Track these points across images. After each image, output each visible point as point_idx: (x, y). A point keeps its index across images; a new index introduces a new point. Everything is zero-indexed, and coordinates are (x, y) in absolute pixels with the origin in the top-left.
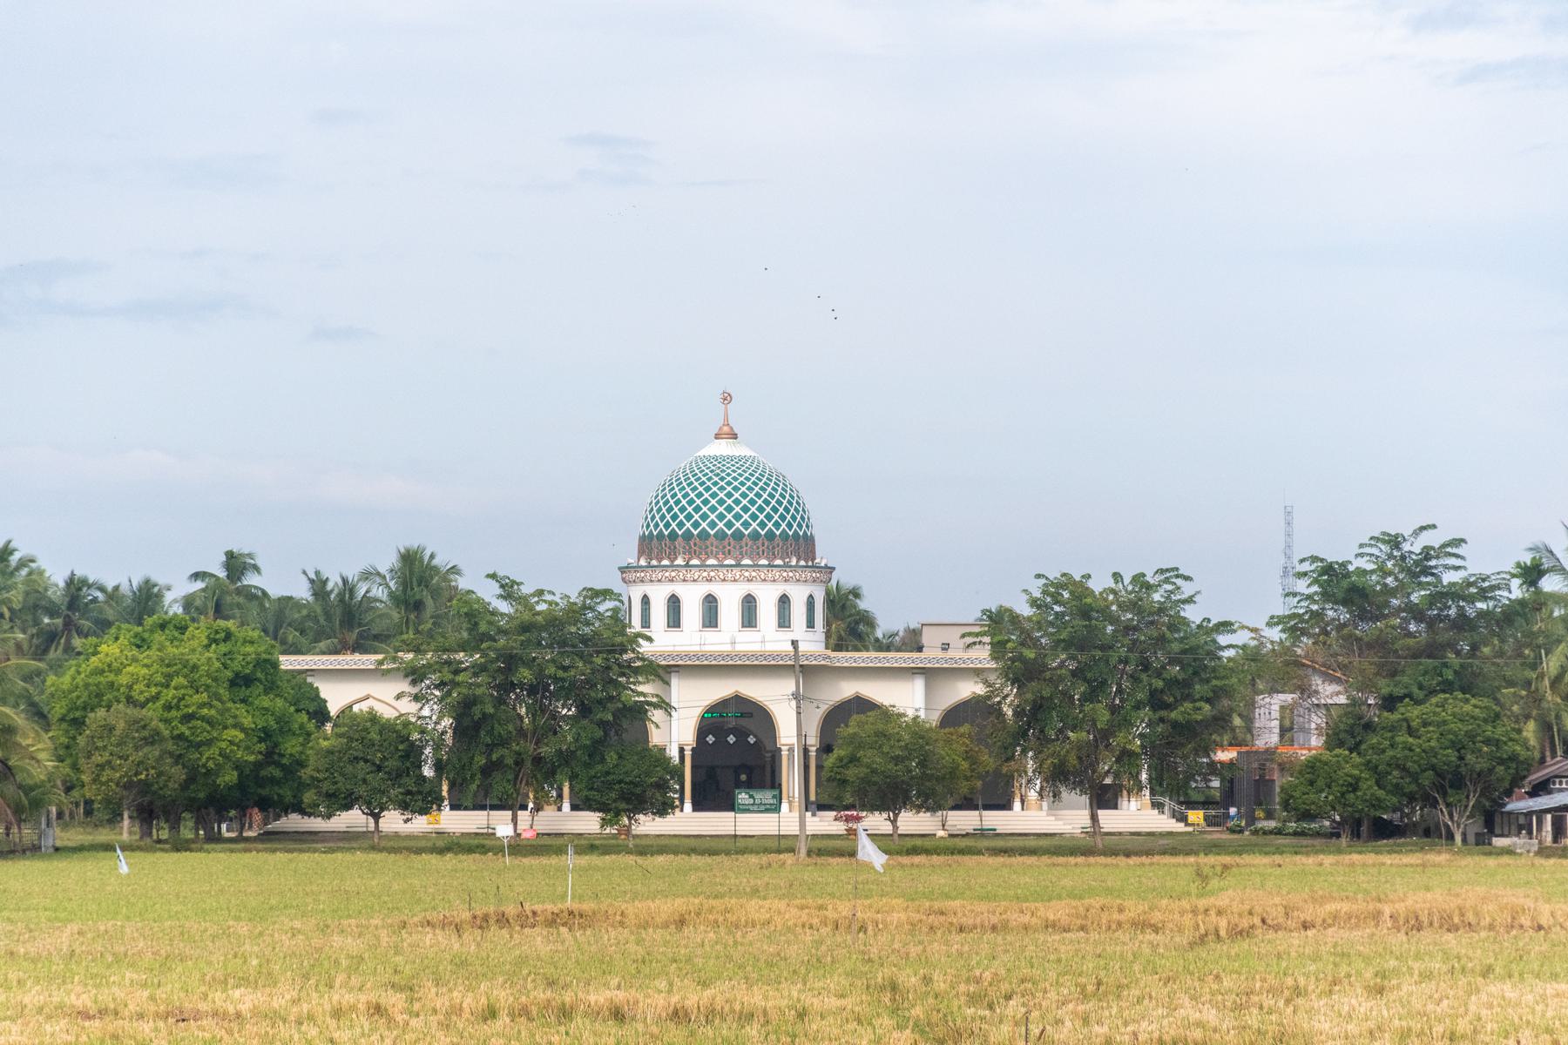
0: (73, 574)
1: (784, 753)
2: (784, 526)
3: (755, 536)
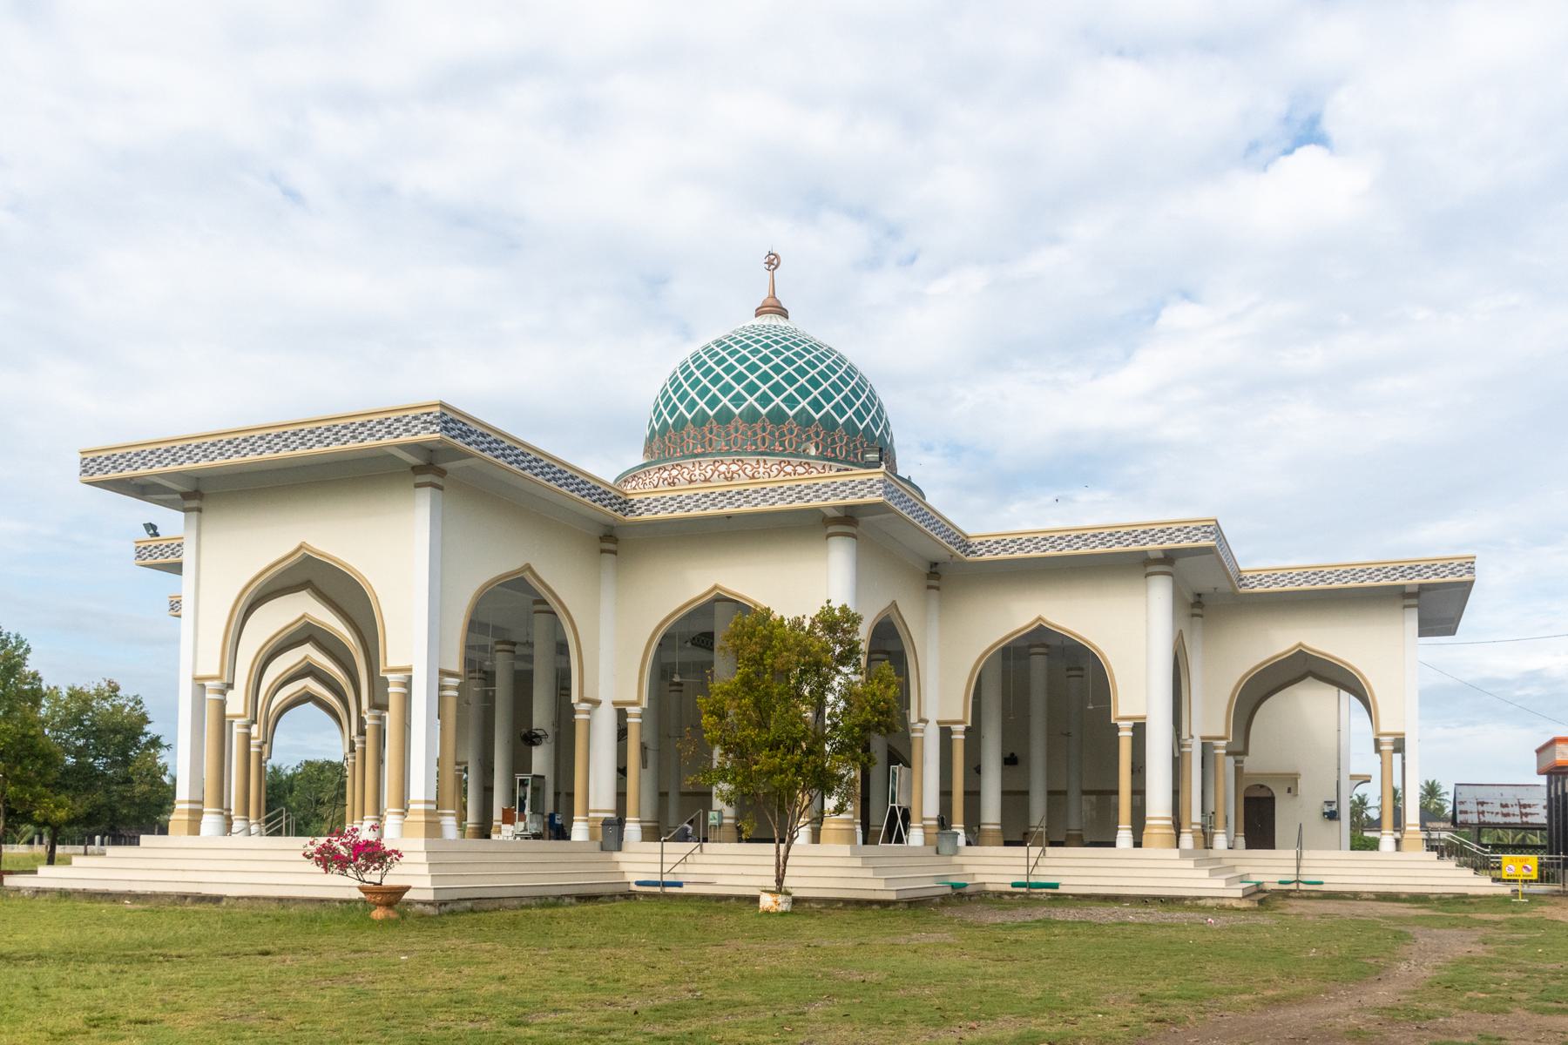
3: (804, 420)
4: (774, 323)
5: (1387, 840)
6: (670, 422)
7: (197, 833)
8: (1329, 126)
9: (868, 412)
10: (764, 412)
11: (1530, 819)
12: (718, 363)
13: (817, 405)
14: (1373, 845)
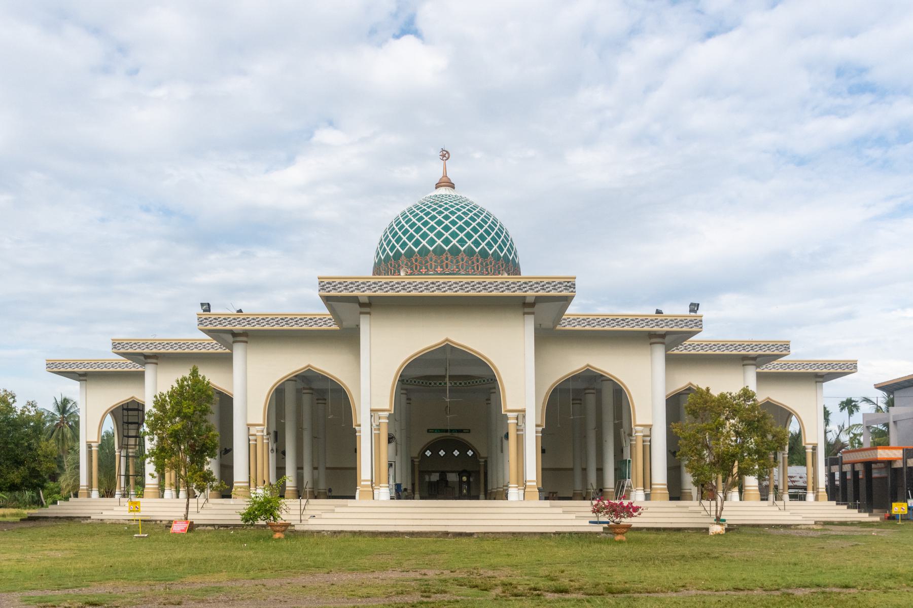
0: (651, 354)
1: (809, 451)
2: (495, 247)
3: (470, 252)
4: (448, 193)
5: (810, 496)
6: (391, 255)
7: (163, 497)
8: (421, 24)
9: (505, 246)
10: (447, 248)
11: (796, 484)
12: (419, 220)
13: (447, 242)
14: (803, 498)
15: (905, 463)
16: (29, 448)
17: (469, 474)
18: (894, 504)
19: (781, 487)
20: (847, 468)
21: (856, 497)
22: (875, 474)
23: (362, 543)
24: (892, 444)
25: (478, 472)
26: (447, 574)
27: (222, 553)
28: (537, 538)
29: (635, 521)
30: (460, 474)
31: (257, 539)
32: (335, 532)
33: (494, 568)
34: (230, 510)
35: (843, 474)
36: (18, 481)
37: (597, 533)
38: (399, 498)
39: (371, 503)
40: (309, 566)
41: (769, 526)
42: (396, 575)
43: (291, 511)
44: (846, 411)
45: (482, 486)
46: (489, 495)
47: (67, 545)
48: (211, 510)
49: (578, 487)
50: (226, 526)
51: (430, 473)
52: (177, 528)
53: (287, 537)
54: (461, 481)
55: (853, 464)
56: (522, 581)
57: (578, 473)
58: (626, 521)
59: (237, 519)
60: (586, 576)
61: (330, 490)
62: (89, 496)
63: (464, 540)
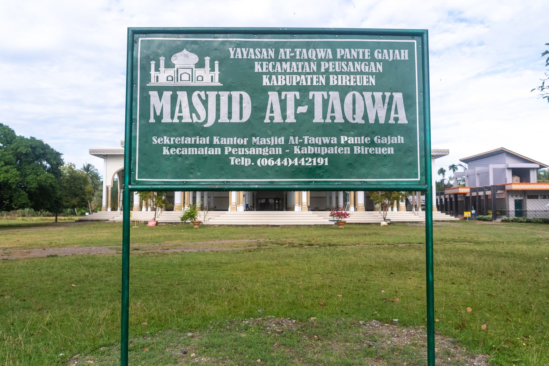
15: (471, 194)
16: (81, 189)
17: (279, 199)
18: (465, 213)
19: (418, 205)
20: (447, 196)
21: (451, 209)
22: (459, 199)
23: (232, 229)
24: (466, 186)
25: (283, 199)
26: (267, 240)
27: (174, 233)
28: (306, 227)
29: (348, 220)
30: (275, 199)
31: (187, 228)
32: (220, 225)
33: (287, 238)
34: (175, 216)
35: (446, 199)
36: (76, 204)
37: (332, 225)
38: (247, 210)
39: (236, 212)
40: (212, 238)
41: (410, 222)
42: (247, 241)
43: (202, 216)
44: (452, 170)
45: (285, 205)
46: (287, 209)
47: (106, 231)
48: (164, 216)
49: (328, 205)
50: (171, 223)
51: (261, 199)
52: (151, 224)
53: (200, 227)
54: (275, 203)
55: (450, 195)
56: (296, 242)
57: (328, 199)
58: (344, 220)
59: (179, 220)
60: (322, 240)
61: (215, 207)
62: (106, 210)
63: (276, 228)
